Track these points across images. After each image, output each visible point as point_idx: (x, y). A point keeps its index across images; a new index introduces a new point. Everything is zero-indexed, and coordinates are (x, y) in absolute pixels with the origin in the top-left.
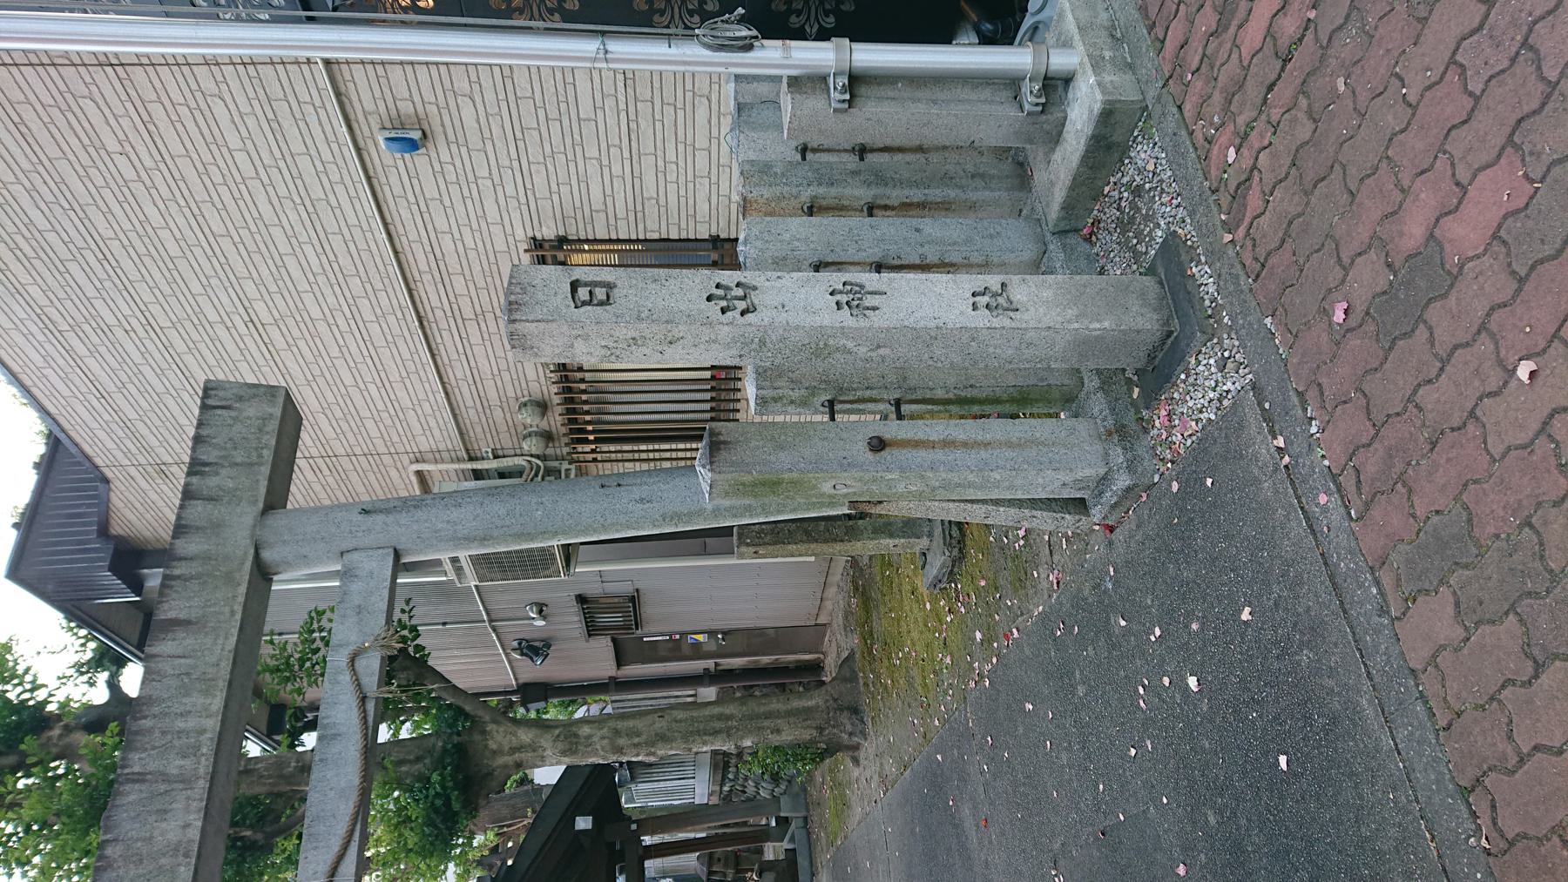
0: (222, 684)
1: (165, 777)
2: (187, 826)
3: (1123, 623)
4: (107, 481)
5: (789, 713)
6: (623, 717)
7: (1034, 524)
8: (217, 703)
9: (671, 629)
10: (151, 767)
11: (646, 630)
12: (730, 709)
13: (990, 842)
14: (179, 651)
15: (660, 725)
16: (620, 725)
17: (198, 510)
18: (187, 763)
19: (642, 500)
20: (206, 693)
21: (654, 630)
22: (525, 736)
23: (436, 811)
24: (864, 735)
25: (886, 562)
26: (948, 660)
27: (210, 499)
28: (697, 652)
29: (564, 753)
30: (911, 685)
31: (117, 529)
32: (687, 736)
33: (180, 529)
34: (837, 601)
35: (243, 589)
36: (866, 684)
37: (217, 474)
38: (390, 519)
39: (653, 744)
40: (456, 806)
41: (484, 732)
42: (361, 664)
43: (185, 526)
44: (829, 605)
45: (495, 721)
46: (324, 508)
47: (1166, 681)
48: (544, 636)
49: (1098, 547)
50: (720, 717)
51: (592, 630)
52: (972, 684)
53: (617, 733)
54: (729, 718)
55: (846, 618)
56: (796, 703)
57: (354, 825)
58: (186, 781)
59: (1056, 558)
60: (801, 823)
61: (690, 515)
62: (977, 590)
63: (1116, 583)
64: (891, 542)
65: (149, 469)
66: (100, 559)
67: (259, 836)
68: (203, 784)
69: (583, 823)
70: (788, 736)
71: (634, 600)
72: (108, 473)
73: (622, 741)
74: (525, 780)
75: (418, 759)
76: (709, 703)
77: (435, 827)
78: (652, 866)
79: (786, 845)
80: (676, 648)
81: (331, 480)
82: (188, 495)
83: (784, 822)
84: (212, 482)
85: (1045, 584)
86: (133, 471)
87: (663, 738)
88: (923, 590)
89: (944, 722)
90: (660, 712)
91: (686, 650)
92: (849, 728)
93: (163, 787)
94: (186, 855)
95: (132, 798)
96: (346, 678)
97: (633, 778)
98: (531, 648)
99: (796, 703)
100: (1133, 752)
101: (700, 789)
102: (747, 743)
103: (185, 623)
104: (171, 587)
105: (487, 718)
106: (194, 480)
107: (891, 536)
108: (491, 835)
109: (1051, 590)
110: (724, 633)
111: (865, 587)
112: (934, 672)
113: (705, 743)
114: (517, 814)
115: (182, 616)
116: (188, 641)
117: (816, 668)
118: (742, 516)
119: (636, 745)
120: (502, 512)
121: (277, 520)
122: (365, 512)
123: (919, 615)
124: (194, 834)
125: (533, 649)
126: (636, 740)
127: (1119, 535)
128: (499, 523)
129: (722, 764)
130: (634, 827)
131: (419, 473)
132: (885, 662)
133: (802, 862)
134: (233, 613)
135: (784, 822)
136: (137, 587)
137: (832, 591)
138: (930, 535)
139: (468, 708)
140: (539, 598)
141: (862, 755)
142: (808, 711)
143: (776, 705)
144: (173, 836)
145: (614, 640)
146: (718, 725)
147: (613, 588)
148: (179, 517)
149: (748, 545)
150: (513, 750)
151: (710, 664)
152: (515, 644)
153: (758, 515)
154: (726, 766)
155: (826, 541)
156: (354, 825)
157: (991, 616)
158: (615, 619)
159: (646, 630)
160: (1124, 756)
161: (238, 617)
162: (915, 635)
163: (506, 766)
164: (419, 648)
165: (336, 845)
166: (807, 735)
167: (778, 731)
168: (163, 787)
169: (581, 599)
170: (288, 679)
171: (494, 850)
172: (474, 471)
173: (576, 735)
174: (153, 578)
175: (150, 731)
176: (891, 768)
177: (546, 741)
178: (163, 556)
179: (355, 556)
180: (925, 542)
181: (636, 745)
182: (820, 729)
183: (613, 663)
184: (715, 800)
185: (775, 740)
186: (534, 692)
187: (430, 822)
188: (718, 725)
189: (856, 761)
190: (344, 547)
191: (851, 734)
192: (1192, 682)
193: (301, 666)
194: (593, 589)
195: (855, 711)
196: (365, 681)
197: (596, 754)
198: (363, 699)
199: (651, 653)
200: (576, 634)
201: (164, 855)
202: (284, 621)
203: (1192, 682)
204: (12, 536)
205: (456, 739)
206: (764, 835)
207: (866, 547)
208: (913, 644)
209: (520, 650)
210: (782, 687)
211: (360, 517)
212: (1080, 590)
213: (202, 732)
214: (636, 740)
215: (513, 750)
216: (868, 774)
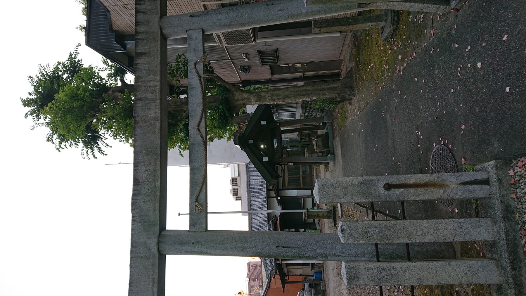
0: (159, 72)
1: (147, 99)
2: (156, 112)
3: (457, 46)
4: (109, 11)
5: (329, 89)
6: (275, 90)
7: (428, 10)
8: (158, 78)
9: (288, 62)
10: (143, 96)
11: (280, 63)
12: (309, 88)
13: (396, 124)
14: (145, 62)
15: (286, 93)
16: (274, 93)
17: (141, 16)
18: (153, 95)
19: (281, 10)
20: (155, 75)
21: (283, 64)
22: (245, 95)
23: (222, 116)
24: (354, 95)
25: (367, 33)
26: (387, 67)
27: (144, 13)
28: (296, 70)
29: (257, 101)
30: (372, 77)
31: (115, 28)
32: (295, 96)
33: (137, 23)
34: (347, 50)
35: (159, 43)
36: (356, 79)
37: (145, 4)
38: (200, 19)
39: (284, 99)
40: (227, 115)
41: (233, 94)
42: (197, 66)
43: (138, 22)
44: (344, 52)
45: (236, 91)
46: (179, 15)
47: (469, 65)
48: (248, 64)
49: (452, 19)
50: (305, 90)
51: (263, 63)
52: (395, 74)
53: (273, 95)
54: (309, 90)
55: (350, 56)
56: (331, 86)
57: (203, 113)
58: (154, 100)
59: (434, 25)
60: (330, 124)
61: (298, 15)
62: (402, 40)
63: (456, 31)
64: (370, 24)
65: (121, 7)
66: (112, 38)
67: (173, 122)
68: (159, 101)
69: (263, 123)
70: (327, 96)
71: (276, 52)
72: (109, 9)
73: (275, 98)
74: (244, 112)
75: (215, 102)
76: (302, 86)
77: (221, 120)
78: (283, 136)
79: (325, 131)
80: (291, 68)
81: (177, 9)
82: (137, 11)
83: (324, 124)
84: (143, 7)
85: (428, 35)
86: (116, 7)
87: (287, 97)
88: (381, 42)
89: (383, 88)
90: (287, 89)
91: (292, 70)
92: (349, 93)
93: (148, 102)
94: (158, 120)
95: (140, 104)
96: (194, 71)
97: (277, 111)
98: (244, 68)
99: (331, 86)
100: (452, 90)
101: (298, 115)
102: (314, 98)
103: (144, 54)
104: (138, 42)
105: (233, 90)
106: (138, 6)
107: (371, 22)
108: (236, 127)
109: (431, 37)
110: (306, 63)
111: (359, 44)
112: (382, 72)
113: (301, 98)
114: (243, 122)
115: (143, 51)
116: (147, 59)
117: (338, 75)
118: (316, 15)
119: (279, 99)
120: (235, 15)
121: (165, 19)
122: (192, 16)
123: (378, 52)
124: (159, 115)
125: (246, 69)
126: (279, 97)
127: (461, 12)
128: (233, 19)
129: (305, 106)
130: (278, 124)
131: (204, 6)
132: (364, 70)
133: (330, 135)
134: (158, 50)
135: (324, 124)
136: (125, 47)
137: (346, 47)
138: (386, 20)
139: (228, 87)
140: (246, 51)
141: (352, 102)
142: (334, 89)
143: (324, 86)
144: (153, 115)
145: (270, 66)
146: (305, 93)
147: (270, 48)
148: (136, 19)
149: (317, 28)
150: (242, 100)
151: (302, 74)
152: (239, 67)
153: (322, 14)
154: (306, 107)
155: (346, 25)
156: (203, 113)
157: (406, 49)
158: (271, 59)
159: (280, 63)
160: (449, 92)
161: (160, 51)
162: (376, 59)
163: (240, 104)
164: (211, 68)
165: (198, 119)
166: (334, 95)
167: (325, 95)
168: (148, 102)
169: (259, 52)
170: (174, 77)
171: (237, 131)
172: (222, 4)
173: (261, 96)
174: (130, 44)
175: (141, 86)
176: (362, 104)
177: (251, 97)
178: (132, 37)
179: (191, 32)
180: (383, 23)
181: (279, 99)
182: (339, 94)
183: (270, 74)
184: (302, 118)
185: (324, 97)
186: (246, 83)
187: (220, 119)
188: (305, 93)
189: (350, 104)
190: (187, 28)
191: (349, 95)
192: (479, 65)
193: (177, 73)
194: (263, 48)
195: (352, 88)
196: (200, 72)
197: (267, 101)
198: (200, 77)
199: (282, 71)
200: (258, 64)
201: (152, 120)
202: (171, 58)
203: (479, 65)
204: (85, 37)
205: (225, 96)
206: (318, 128)
207: (361, 27)
208: (375, 63)
209: (241, 69)
210: (326, 82)
211: (190, 18)
212: (442, 35)
213: (156, 86)
214: (279, 97)
215: (242, 100)
216: (354, 107)
